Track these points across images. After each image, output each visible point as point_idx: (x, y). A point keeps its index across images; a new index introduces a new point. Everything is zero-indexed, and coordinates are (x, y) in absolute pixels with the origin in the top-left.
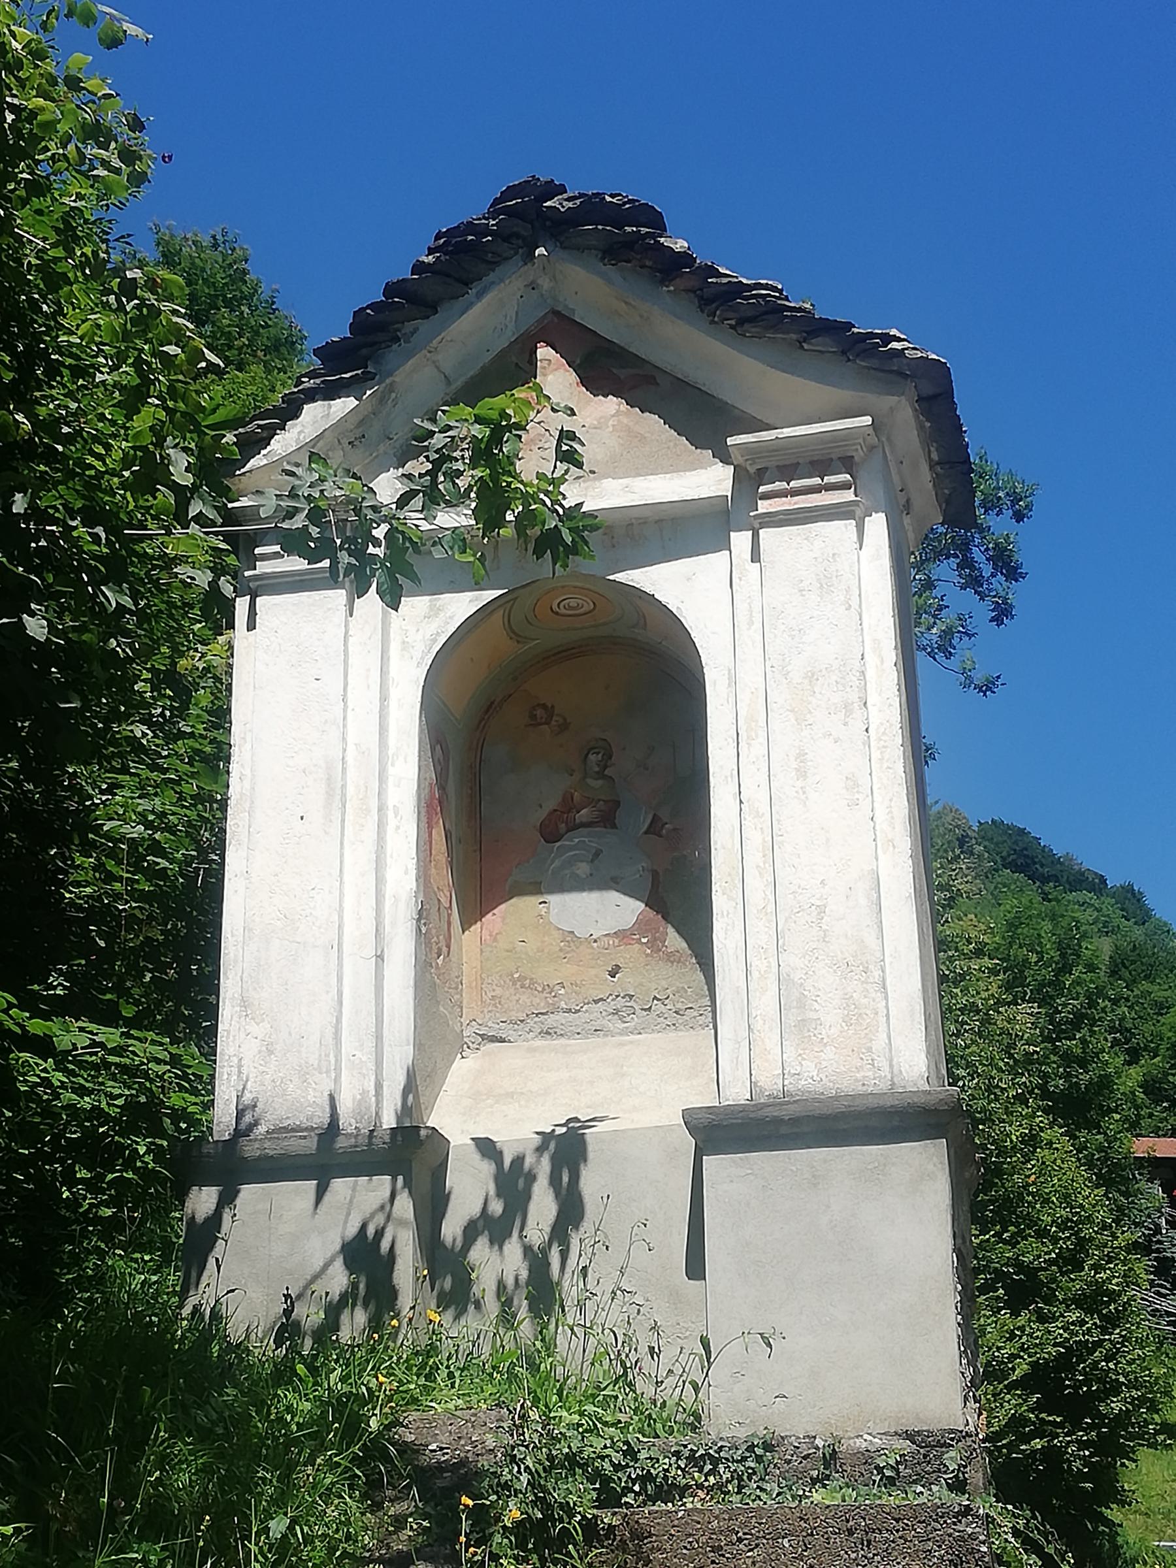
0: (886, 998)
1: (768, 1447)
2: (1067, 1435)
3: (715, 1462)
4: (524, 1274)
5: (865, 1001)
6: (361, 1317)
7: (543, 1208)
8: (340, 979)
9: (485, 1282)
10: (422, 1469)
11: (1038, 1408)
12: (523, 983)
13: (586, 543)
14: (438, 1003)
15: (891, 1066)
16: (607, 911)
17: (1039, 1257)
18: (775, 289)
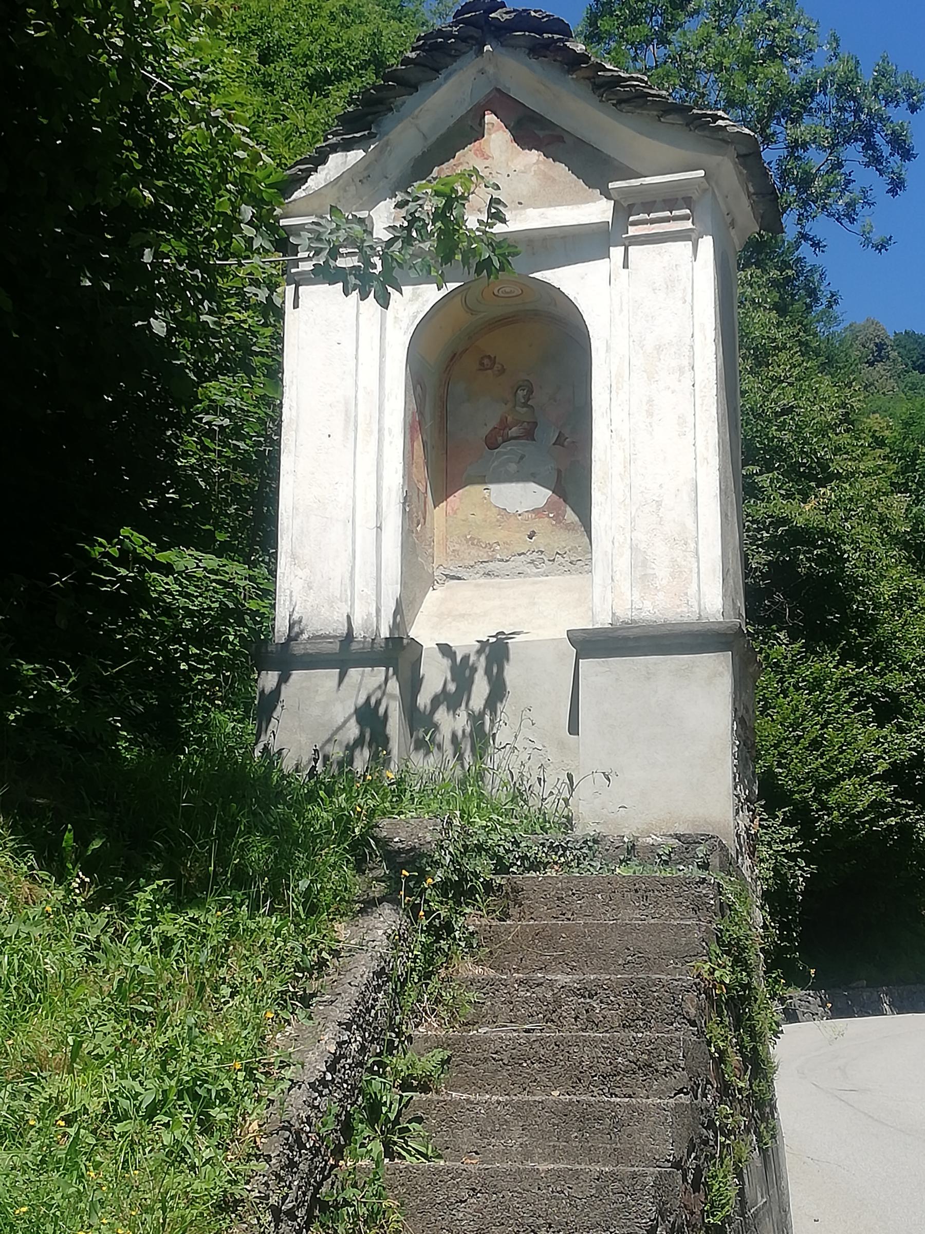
0: (698, 562)
1: (595, 841)
2: (917, 814)
3: (565, 849)
4: (468, 729)
5: (684, 563)
6: (366, 753)
7: (481, 689)
8: (354, 542)
9: (445, 735)
10: (390, 852)
11: (896, 793)
12: (473, 542)
13: (510, 264)
14: (417, 556)
15: (699, 605)
16: (528, 496)
17: (901, 685)
18: (642, 81)
